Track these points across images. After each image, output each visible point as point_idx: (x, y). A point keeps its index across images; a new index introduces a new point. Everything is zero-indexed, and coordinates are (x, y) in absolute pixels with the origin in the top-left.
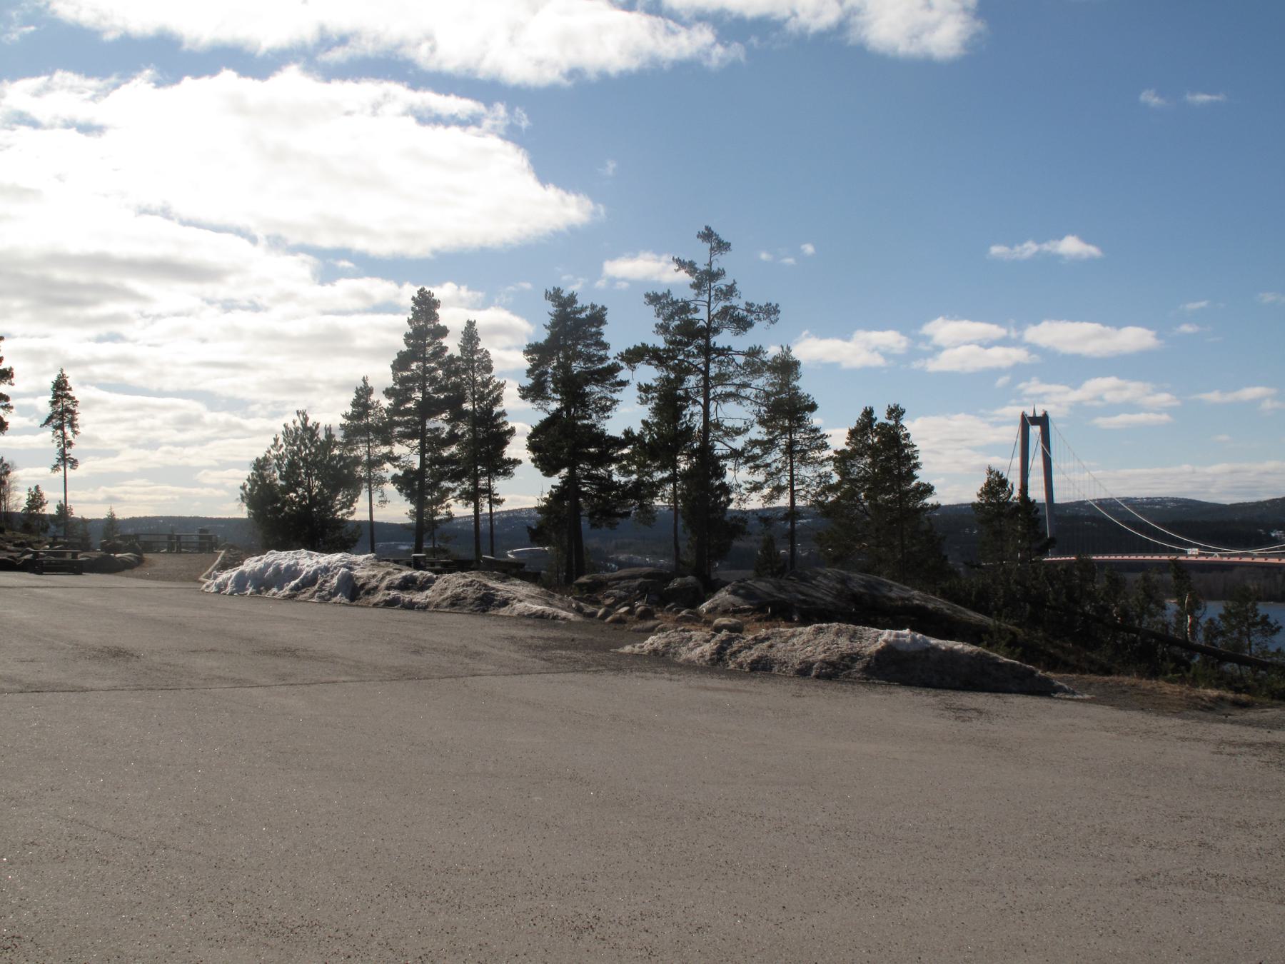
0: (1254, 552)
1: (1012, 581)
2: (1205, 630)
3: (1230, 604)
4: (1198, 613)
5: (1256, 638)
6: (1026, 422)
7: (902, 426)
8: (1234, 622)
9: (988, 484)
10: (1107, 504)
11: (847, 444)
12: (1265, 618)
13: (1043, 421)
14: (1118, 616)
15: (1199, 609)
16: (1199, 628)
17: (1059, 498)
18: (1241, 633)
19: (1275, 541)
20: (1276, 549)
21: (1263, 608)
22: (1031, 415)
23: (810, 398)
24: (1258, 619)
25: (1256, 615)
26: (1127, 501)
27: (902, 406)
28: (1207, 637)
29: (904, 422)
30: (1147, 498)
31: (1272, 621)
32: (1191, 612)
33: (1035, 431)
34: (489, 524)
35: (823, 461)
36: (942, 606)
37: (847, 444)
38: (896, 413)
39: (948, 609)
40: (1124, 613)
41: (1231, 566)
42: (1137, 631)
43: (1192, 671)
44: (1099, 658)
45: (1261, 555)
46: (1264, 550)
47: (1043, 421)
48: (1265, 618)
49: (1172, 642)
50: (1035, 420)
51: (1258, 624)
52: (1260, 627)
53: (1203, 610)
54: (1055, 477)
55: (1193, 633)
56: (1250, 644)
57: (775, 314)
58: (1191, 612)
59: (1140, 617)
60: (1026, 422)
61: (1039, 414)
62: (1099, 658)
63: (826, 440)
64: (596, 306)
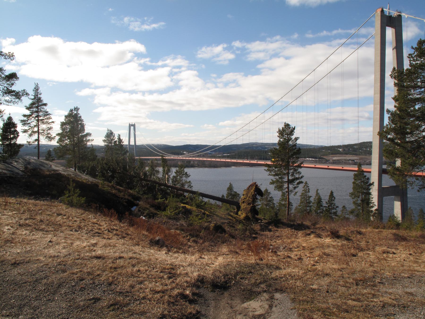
0: (180, 156)
2: (172, 179)
4: (169, 174)
5: (184, 178)
6: (130, 125)
7: (79, 113)
8: (178, 174)
9: (107, 134)
10: (149, 146)
12: (186, 173)
13: (134, 126)
15: (170, 172)
17: (138, 143)
18: (180, 177)
19: (184, 154)
20: (195, 154)
21: (186, 170)
22: (131, 124)
23: (26, 91)
24: (184, 173)
25: (184, 172)
27: (78, 107)
31: (188, 173)
33: (132, 128)
34: (37, 150)
35: (50, 123)
39: (73, 175)
40: (145, 174)
41: (176, 159)
42: (149, 181)
43: (168, 200)
44: (134, 192)
45: (182, 157)
47: (134, 126)
48: (186, 173)
49: (160, 185)
50: (132, 125)
52: (185, 175)
53: (171, 172)
55: (168, 181)
56: (182, 180)
58: (167, 174)
59: (151, 175)
60: (130, 125)
61: (133, 124)
62: (134, 192)
63: (50, 116)
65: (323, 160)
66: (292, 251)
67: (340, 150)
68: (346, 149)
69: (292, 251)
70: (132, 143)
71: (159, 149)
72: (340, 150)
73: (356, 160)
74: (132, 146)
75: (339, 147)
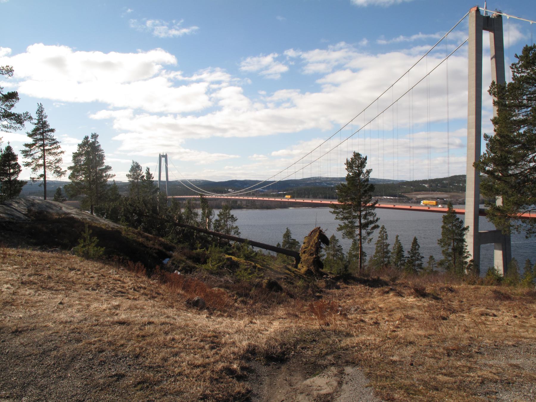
0: (224, 195)
1: (128, 204)
3: (221, 210)
4: (211, 217)
6: (161, 156)
9: (132, 167)
10: (185, 182)
11: (78, 150)
13: (165, 157)
14: (177, 219)
15: (211, 215)
16: (211, 223)
17: (170, 179)
19: (229, 192)
20: (243, 192)
23: (29, 114)
24: (230, 216)
25: (229, 215)
26: (189, 180)
28: (215, 227)
29: (98, 140)
30: (156, 50)
31: (234, 216)
32: (208, 217)
33: (163, 159)
36: (86, 217)
37: (78, 150)
38: (95, 136)
39: (89, 219)
40: (180, 218)
41: (218, 199)
42: (185, 226)
45: (226, 196)
46: (226, 195)
47: (165, 157)
49: (200, 231)
50: (163, 156)
51: (230, 218)
52: (230, 219)
53: (213, 215)
54: (169, 173)
55: (209, 226)
57: (11, 71)
58: (208, 217)
60: (161, 156)
61: (165, 154)
64: (48, 126)
65: (404, 198)
66: (366, 313)
67: (426, 185)
68: (434, 185)
69: (366, 313)
70: (163, 179)
71: (197, 186)
72: (426, 185)
73: (446, 198)
74: (164, 182)
75: (425, 182)
